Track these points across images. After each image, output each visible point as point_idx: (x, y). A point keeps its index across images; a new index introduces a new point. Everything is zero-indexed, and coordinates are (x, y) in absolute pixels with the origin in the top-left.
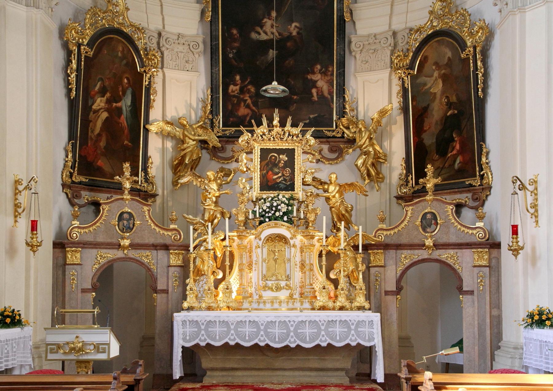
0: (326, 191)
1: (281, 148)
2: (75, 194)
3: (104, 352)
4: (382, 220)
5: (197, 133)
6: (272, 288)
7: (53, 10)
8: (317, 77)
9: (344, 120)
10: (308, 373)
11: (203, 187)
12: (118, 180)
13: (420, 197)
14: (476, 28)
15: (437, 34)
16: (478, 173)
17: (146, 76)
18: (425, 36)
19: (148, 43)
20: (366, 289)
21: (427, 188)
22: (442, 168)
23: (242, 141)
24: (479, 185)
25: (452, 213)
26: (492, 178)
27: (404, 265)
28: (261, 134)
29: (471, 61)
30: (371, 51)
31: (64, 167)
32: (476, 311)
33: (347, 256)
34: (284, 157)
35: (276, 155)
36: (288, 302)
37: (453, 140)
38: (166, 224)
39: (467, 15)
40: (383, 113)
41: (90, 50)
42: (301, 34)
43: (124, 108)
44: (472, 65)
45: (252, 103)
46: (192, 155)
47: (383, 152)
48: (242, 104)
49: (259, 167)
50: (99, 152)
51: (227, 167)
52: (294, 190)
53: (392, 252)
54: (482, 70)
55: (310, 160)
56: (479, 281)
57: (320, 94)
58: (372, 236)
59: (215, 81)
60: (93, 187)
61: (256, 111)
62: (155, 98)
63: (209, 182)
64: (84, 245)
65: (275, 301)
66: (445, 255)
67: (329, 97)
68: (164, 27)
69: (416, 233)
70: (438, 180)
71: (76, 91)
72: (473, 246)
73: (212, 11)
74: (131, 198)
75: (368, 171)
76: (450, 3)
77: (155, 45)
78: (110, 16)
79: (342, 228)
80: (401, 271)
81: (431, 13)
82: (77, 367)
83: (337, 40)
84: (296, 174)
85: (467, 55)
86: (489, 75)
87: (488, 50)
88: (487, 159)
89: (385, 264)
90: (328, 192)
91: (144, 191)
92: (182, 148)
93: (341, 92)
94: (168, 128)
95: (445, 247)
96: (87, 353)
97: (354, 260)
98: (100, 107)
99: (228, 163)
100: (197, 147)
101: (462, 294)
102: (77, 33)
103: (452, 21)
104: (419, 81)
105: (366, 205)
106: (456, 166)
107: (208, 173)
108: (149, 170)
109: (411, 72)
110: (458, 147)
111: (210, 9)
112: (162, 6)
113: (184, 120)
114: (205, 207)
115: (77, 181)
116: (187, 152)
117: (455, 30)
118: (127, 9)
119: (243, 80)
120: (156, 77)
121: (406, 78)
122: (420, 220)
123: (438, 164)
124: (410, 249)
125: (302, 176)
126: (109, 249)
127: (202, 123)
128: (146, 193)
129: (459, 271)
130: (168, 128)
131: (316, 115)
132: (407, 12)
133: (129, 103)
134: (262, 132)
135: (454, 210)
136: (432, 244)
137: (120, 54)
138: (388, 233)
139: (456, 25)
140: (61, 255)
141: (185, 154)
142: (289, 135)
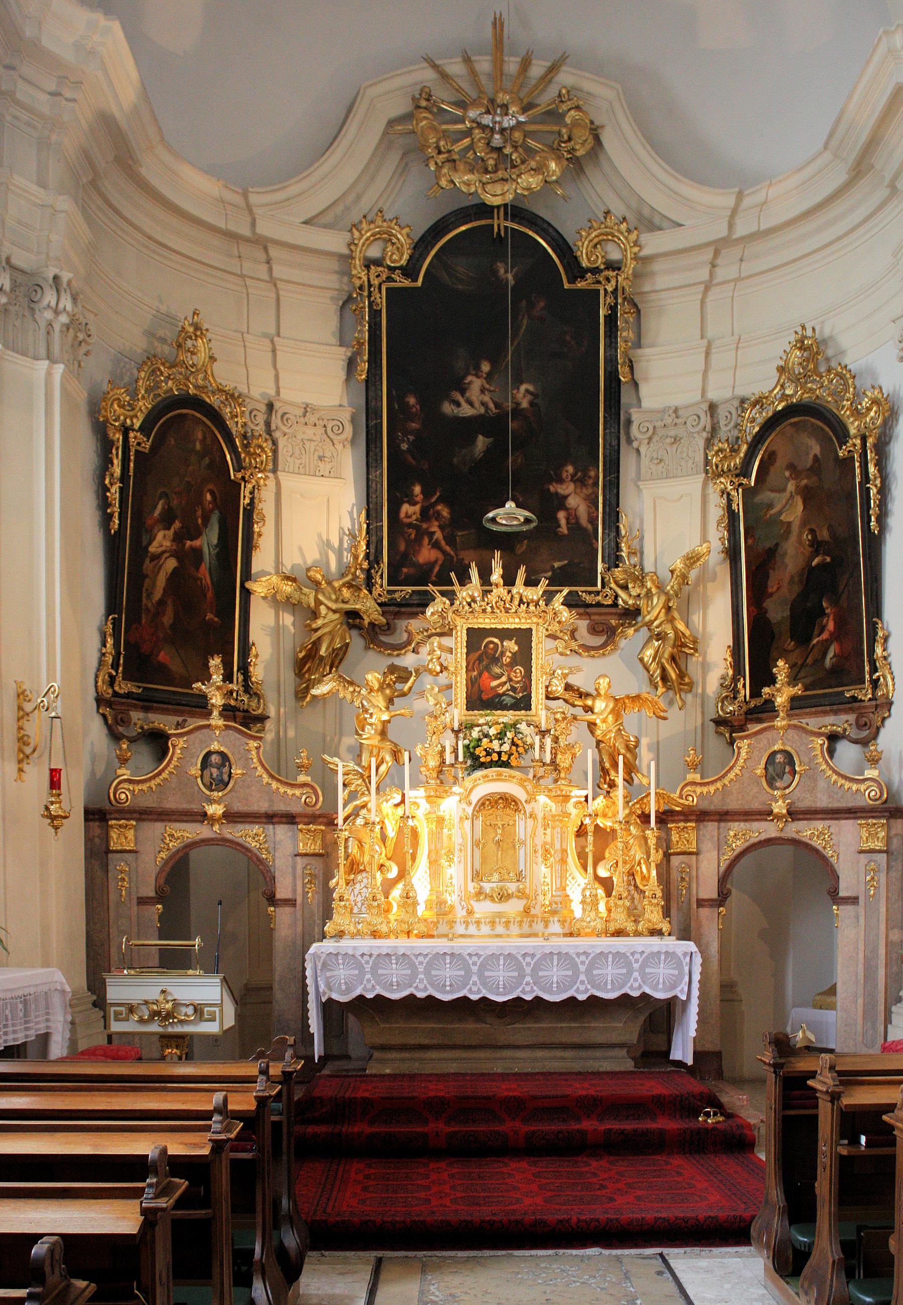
0: (589, 709)
1: (505, 627)
2: (119, 717)
3: (213, 1020)
4: (694, 767)
5: (341, 598)
6: (492, 896)
7: (83, 364)
8: (566, 489)
9: (618, 572)
10: (559, 1053)
11: (357, 703)
12: (201, 690)
13: (760, 721)
14: (866, 402)
15: (792, 410)
16: (867, 676)
17: (245, 487)
18: (770, 414)
19: (250, 423)
20: (662, 897)
21: (776, 704)
22: (802, 665)
23: (433, 614)
24: (870, 700)
25: (822, 752)
26: (894, 685)
27: (733, 849)
28: (469, 600)
29: (857, 464)
30: (669, 440)
31: (100, 665)
32: (862, 933)
33: (631, 834)
34: (511, 646)
35: (496, 640)
36: (521, 922)
37: (822, 613)
38: (283, 772)
39: (848, 376)
40: (692, 560)
41: (145, 439)
42: (536, 405)
43: (206, 550)
44: (858, 471)
45: (445, 538)
46: (332, 640)
47: (690, 635)
48: (426, 541)
49: (464, 664)
50: (161, 635)
51: (398, 662)
52: (530, 709)
53: (711, 827)
54: (878, 482)
55: (560, 650)
56: (868, 878)
57: (573, 521)
58: (676, 796)
59: (374, 496)
60: (147, 702)
61: (452, 553)
62: (263, 530)
63: (369, 693)
64: (143, 815)
65: (497, 920)
66: (807, 831)
67: (589, 527)
68: (278, 393)
69: (755, 790)
70: (798, 690)
71: (120, 519)
72: (859, 815)
73: (369, 361)
74: (224, 725)
75: (664, 669)
76: (818, 353)
77: (260, 429)
78: (181, 373)
79: (620, 781)
80: (728, 861)
81: (781, 370)
82: (162, 1046)
83: (605, 417)
84: (533, 678)
85: (849, 451)
86: (889, 490)
87: (887, 443)
88: (884, 650)
89: (697, 848)
90: (593, 712)
91: (244, 711)
92: (314, 626)
93: (613, 518)
94: (288, 588)
95: (808, 816)
96: (181, 1022)
97: (643, 842)
98: (163, 548)
99: (398, 655)
100: (341, 623)
101: (837, 904)
102: (122, 406)
103: (822, 387)
104: (758, 499)
105: (658, 736)
106: (828, 662)
107: (369, 677)
108: (251, 669)
109: (745, 481)
110: (831, 626)
111: (366, 358)
112: (274, 351)
113: (316, 571)
114: (362, 741)
115: (122, 692)
116: (323, 635)
117: (827, 405)
118: (212, 359)
119: (426, 493)
120: (263, 488)
121: (734, 493)
122: (763, 765)
123: (793, 657)
124: (745, 821)
125: (544, 680)
126: (187, 821)
127: (350, 577)
128: (246, 714)
129: (834, 860)
130: (288, 588)
131: (566, 562)
132: (736, 367)
133: (215, 541)
134: (471, 596)
135: (826, 746)
136: (784, 811)
137: (198, 446)
138: (705, 790)
139: (828, 395)
140: (98, 831)
141: (319, 638)
142: (521, 602)
